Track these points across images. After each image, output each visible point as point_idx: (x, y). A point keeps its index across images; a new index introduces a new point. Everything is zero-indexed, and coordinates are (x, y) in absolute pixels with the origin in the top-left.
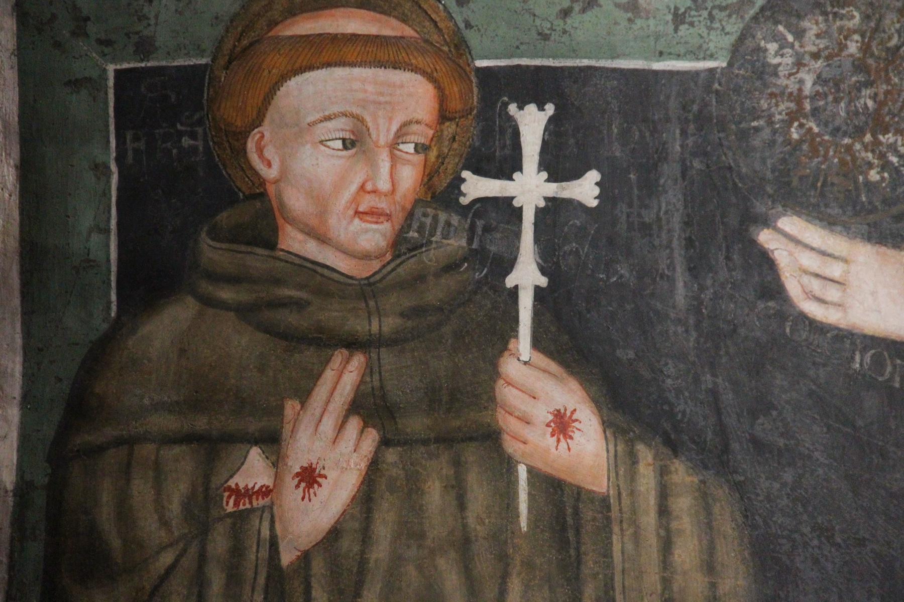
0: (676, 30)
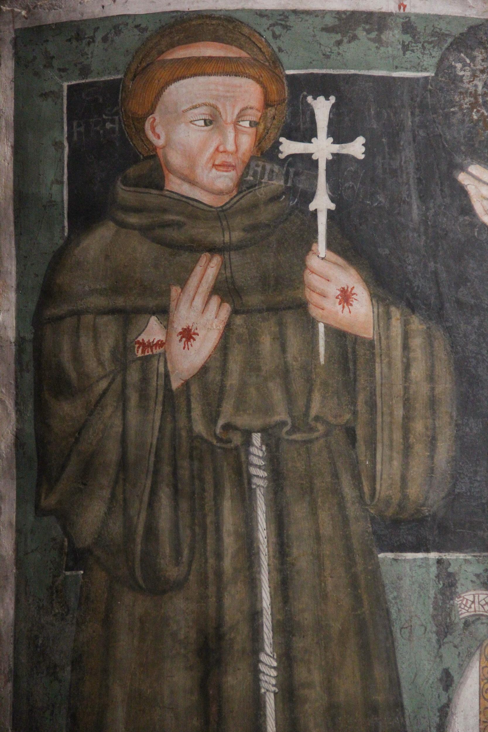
0: (404, 54)
